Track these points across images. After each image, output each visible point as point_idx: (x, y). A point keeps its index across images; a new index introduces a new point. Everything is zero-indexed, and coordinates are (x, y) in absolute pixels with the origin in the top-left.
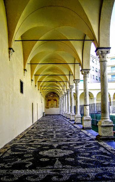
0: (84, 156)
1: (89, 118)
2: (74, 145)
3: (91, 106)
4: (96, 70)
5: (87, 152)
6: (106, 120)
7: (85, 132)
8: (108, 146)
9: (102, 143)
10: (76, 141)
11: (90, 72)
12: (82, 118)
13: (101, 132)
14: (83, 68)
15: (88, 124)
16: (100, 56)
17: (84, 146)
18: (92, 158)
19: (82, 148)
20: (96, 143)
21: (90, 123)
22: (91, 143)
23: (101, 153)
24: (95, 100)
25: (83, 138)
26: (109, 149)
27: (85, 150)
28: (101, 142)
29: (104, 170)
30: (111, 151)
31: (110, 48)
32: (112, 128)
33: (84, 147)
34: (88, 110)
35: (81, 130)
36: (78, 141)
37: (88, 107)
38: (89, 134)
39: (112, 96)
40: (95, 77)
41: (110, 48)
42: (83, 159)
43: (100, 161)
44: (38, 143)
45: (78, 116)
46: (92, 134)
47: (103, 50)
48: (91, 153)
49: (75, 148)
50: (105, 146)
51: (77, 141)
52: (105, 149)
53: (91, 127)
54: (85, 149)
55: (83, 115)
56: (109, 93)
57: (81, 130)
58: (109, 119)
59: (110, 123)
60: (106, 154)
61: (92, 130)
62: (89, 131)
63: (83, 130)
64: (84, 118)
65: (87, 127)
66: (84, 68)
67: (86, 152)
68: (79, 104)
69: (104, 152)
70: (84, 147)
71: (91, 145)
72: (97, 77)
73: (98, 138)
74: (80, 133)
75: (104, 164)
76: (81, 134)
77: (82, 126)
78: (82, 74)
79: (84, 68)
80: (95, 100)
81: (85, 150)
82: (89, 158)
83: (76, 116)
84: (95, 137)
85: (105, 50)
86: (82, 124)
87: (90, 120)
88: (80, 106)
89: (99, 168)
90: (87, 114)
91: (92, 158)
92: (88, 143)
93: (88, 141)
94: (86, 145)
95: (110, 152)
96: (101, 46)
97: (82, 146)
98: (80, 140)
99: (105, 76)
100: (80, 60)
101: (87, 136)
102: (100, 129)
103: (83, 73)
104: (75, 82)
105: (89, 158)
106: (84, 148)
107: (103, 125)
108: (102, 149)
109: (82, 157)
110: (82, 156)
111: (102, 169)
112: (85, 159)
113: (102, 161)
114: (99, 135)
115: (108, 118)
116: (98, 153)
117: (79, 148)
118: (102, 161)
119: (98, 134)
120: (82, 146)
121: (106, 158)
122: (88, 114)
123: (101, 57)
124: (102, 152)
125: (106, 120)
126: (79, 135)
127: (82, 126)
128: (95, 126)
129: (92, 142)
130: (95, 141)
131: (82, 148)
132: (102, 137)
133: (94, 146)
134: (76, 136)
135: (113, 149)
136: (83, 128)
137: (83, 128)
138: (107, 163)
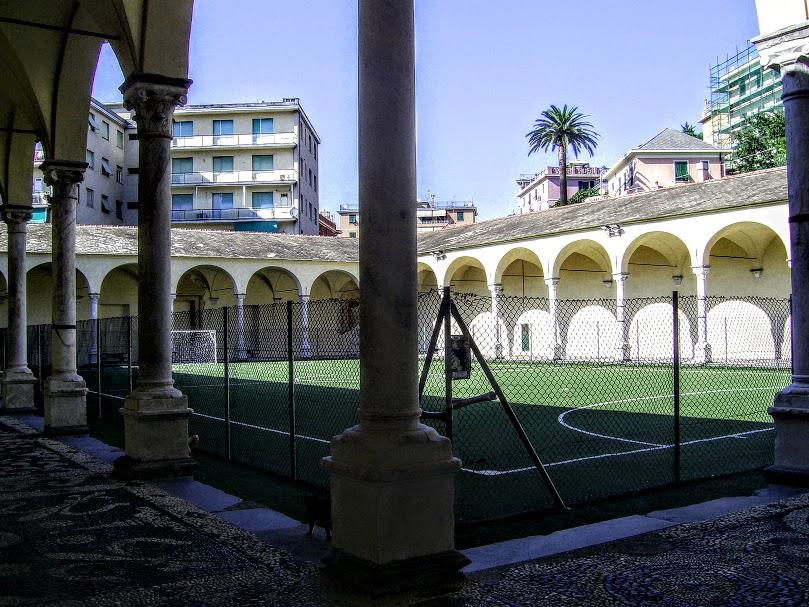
0: (75, 549)
1: (78, 384)
2: (17, 509)
3: (84, 327)
4: (105, 165)
5: (87, 533)
6: (158, 391)
7: (60, 447)
8: (175, 503)
9: (144, 491)
10: (23, 490)
11: (85, 174)
12: (36, 385)
13: (138, 445)
14: (53, 156)
15: (76, 412)
16: (144, 112)
17: (68, 509)
18: (108, 553)
19: (58, 517)
20: (116, 490)
21: (80, 407)
22: (94, 492)
23: (149, 530)
24: (95, 306)
25: (52, 475)
26: (179, 513)
27: (70, 523)
28: (139, 485)
29: (168, 595)
30: (189, 520)
31: (190, 82)
32: (186, 423)
33: (66, 511)
34: (74, 350)
35: (40, 440)
36: (35, 487)
37: (72, 336)
38: (80, 458)
39: (95, 286)
40: (98, 200)
41: (190, 82)
42: (71, 561)
43: (149, 562)
44: (94, 488)
45: (20, 377)
46: (95, 454)
47: (157, 87)
48: (100, 534)
49: (22, 519)
50: (158, 501)
51: (29, 489)
52: (162, 511)
53: (85, 423)
54: (72, 518)
55: (45, 369)
56: (80, 275)
57: (40, 440)
58: (172, 387)
59: (178, 402)
60: (166, 532)
61: (90, 440)
62: (79, 442)
63: (48, 442)
64: (55, 385)
65: (64, 424)
66: (59, 156)
67: (81, 532)
68: (24, 323)
69: (158, 523)
70: (66, 511)
71: (96, 503)
72: (104, 197)
73: (126, 469)
74: (37, 453)
75: (166, 570)
76: (41, 459)
77: (40, 422)
78: (48, 181)
79: (59, 156)
80: (95, 306)
81: (70, 523)
82: (98, 556)
83: (8, 379)
84: (109, 468)
85: (165, 88)
86: (42, 415)
87: (81, 394)
88: (28, 327)
89: (145, 587)
90: (65, 368)
91: (108, 553)
92: (83, 494)
93: (79, 485)
94: (76, 502)
95: (186, 525)
96: (150, 68)
97: (54, 510)
98: (43, 485)
99: (162, 200)
100: (40, 117)
101: (74, 465)
102: (131, 427)
103: (54, 176)
104: (9, 216)
105: (98, 556)
106: (67, 518)
107: (146, 412)
108: (146, 515)
109: (62, 556)
110: (65, 548)
111: (162, 592)
112: (81, 560)
113: (156, 561)
114: (126, 459)
115: (166, 380)
116: (131, 532)
117: (41, 520)
118: (156, 561)
119: (123, 454)
120: (54, 510)
121: (169, 549)
122: (74, 366)
123: (148, 116)
124: (148, 525)
125: (158, 391)
126: (34, 461)
127: (40, 422)
128: (104, 420)
129: (102, 487)
130: (110, 483)
131: (58, 517)
132: (145, 466)
133: (112, 506)
134: (19, 469)
135: (193, 509)
136: (51, 432)
137: (51, 432)
138: (176, 566)
